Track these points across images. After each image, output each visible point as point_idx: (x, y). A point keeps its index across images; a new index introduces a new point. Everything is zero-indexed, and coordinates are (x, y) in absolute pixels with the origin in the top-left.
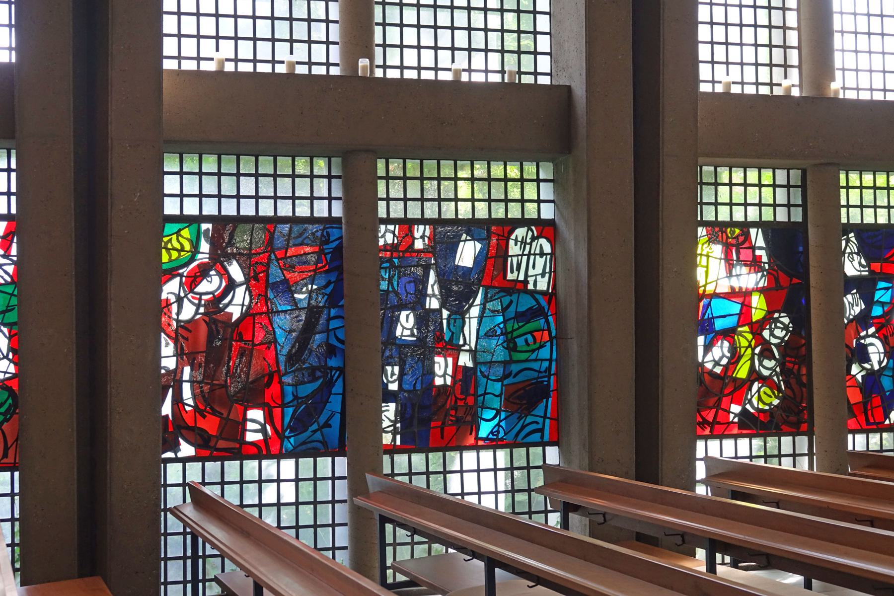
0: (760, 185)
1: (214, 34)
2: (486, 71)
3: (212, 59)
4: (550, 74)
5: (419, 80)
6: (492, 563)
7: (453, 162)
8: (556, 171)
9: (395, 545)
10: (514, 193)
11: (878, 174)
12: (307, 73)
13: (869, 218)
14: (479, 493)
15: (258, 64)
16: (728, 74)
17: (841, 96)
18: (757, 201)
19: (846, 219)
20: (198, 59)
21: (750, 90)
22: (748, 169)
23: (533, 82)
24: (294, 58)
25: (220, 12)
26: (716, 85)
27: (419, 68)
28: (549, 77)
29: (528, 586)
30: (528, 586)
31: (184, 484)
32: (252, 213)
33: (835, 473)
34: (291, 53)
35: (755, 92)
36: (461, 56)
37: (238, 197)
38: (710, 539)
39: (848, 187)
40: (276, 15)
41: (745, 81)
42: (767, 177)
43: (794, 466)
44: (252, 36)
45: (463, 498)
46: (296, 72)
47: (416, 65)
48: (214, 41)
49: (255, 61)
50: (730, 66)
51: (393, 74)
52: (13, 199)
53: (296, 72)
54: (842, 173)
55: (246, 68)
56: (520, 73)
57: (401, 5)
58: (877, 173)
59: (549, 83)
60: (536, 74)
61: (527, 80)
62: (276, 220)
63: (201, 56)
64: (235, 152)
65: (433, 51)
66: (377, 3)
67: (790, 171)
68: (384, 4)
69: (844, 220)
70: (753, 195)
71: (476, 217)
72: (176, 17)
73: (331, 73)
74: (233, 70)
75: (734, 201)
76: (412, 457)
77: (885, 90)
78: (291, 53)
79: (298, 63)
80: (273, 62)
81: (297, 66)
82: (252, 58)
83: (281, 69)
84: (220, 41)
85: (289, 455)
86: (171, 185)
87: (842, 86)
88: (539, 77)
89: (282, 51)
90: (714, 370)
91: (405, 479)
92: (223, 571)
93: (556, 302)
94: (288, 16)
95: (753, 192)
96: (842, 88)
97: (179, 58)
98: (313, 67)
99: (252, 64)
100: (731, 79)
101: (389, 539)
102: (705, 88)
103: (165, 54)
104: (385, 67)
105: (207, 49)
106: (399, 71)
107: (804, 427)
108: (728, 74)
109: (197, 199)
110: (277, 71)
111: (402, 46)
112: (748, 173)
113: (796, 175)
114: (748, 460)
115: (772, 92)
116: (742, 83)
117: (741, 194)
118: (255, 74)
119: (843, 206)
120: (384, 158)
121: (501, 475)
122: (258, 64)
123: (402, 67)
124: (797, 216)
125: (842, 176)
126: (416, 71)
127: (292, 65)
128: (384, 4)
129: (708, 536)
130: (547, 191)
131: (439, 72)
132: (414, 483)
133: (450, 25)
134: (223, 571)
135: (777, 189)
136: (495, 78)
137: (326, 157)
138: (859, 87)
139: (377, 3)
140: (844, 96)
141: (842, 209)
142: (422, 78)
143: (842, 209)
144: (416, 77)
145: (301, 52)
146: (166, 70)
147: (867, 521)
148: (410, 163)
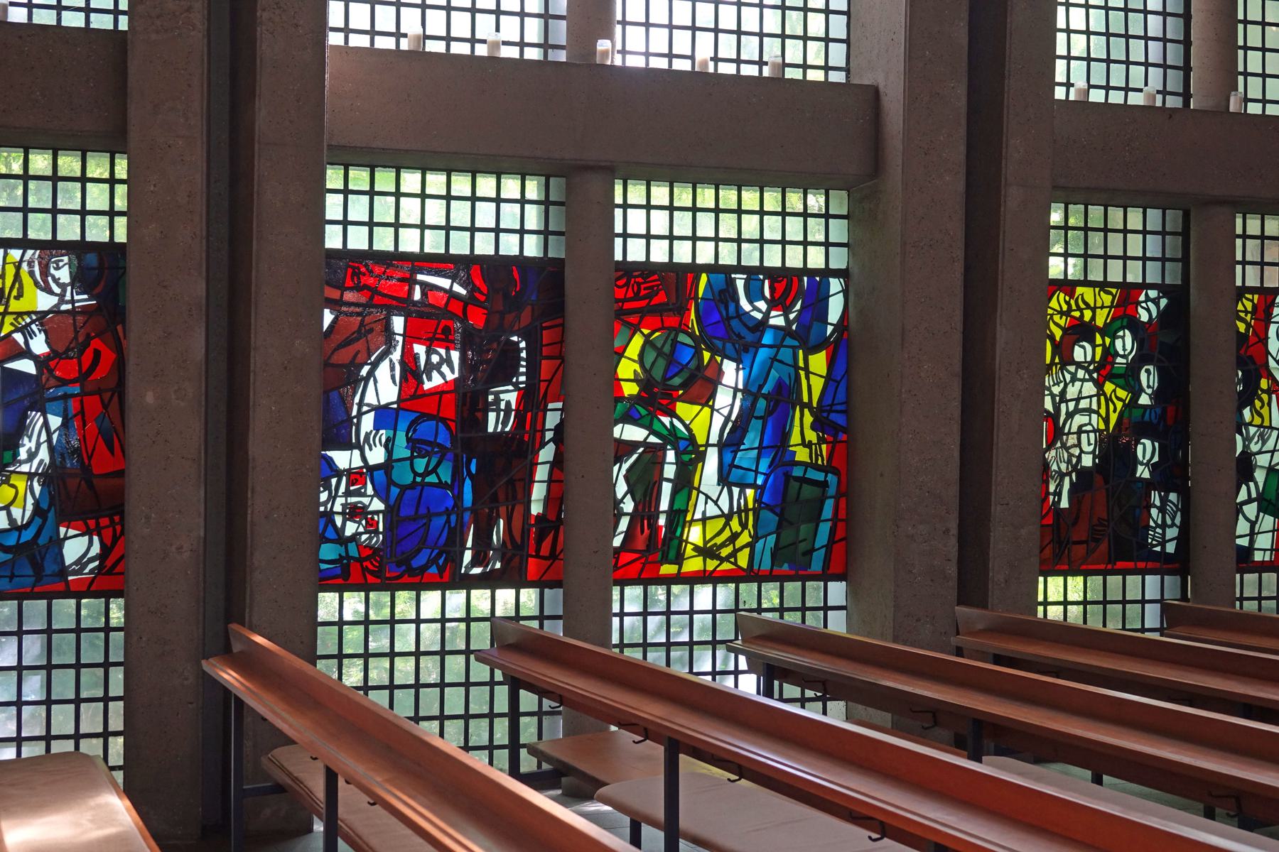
1: (667, 22)
2: (647, 54)
5: (1125, 106)
6: (675, 746)
7: (1102, 208)
13: (484, 246)
15: (742, 66)
17: (711, 70)
19: (116, 224)
21: (816, 76)
24: (504, 36)
28: (844, 74)
32: (415, 248)
33: (868, 637)
34: (498, 30)
36: (705, 40)
39: (1245, 236)
42: (816, 201)
43: (1105, 625)
45: (622, 651)
47: (469, 36)
54: (619, 184)
56: (716, 59)
57: (1087, 6)
58: (89, 154)
61: (436, 47)
64: (1103, 203)
65: (712, 35)
66: (1061, 4)
67: (1167, 211)
68: (1068, 5)
73: (526, 56)
75: (1129, 254)
77: (1264, 101)
78: (498, 30)
79: (505, 43)
80: (473, 41)
81: (11, 9)
83: (481, 50)
84: (628, 27)
86: (333, 209)
87: (713, 56)
88: (453, 44)
91: (535, 624)
93: (847, 389)
95: (773, 224)
96: (712, 59)
98: (377, 38)
99: (734, 65)
106: (734, 65)
107: (484, 564)
109: (493, 235)
110: (1267, 113)
112: (653, 189)
113: (1174, 217)
114: (777, 615)
115: (647, 63)
120: (393, 167)
123: (373, 33)
124: (557, 250)
125: (1239, 221)
126: (517, 49)
127: (495, 46)
128: (1068, 5)
130: (839, 231)
131: (628, 57)
137: (542, 175)
139: (1061, 4)
140: (612, 61)
141: (616, 239)
143: (616, 239)
145: (705, 43)
147: (927, 712)
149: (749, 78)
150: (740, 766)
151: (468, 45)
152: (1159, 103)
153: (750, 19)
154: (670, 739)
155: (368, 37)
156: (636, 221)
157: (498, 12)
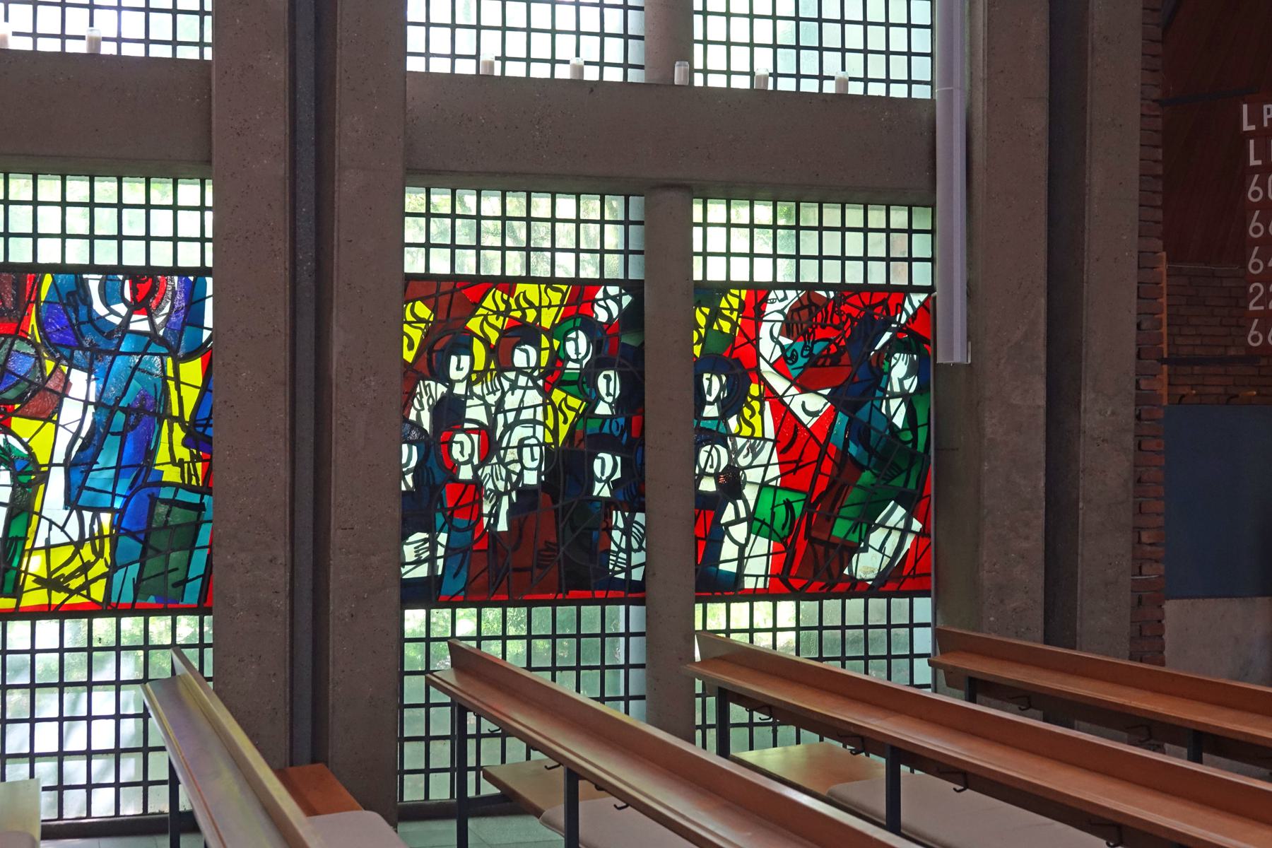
0: (865, 230)
3: (82, 38)
4: (931, 83)
6: (899, 754)
8: (648, 208)
9: (479, 736)
10: (899, 248)
11: (183, 183)
12: (794, 89)
14: (554, 669)
15: (152, 46)
16: (6, 19)
17: (497, 72)
18: (422, 240)
20: (63, 37)
22: (891, 207)
23: (794, 89)
25: (846, 18)
26: (825, 82)
27: (798, 76)
29: (615, 806)
30: (615, 806)
31: (173, 645)
35: (59, 50)
37: (148, 238)
38: (1195, 731)
40: (869, 19)
41: (709, 67)
44: (862, 47)
46: (585, 79)
47: (725, 68)
48: (862, 55)
49: (174, 43)
50: (709, 46)
51: (717, 81)
52: (209, 246)
53: (850, 92)
55: (877, 90)
59: (748, 86)
60: (798, 76)
61: (787, 85)
62: (36, 269)
63: (606, 60)
64: (525, 188)
69: (698, 276)
70: (854, 244)
71: (870, 282)
72: (771, 21)
74: (596, 78)
76: (66, 624)
81: (851, 83)
82: (906, 78)
85: (188, 611)
86: (413, 231)
89: (832, 62)
90: (177, 498)
92: (503, 761)
94: (883, 20)
96: (771, 75)
97: (427, 55)
100: (585, 55)
101: (471, 730)
102: (415, 65)
103: (409, 50)
104: (705, 72)
105: (832, 62)
108: (6, 19)
110: (870, 93)
111: (602, 35)
116: (119, 40)
117: (409, 227)
118: (147, 61)
119: (698, 254)
121: (563, 644)
122: (152, 46)
127: (843, 83)
129: (1194, 727)
132: (483, 649)
133: (905, 22)
134: (503, 761)
135: (914, 236)
136: (742, 83)
138: (123, 36)
142: (151, 55)
144: (724, 85)
146: (411, 72)
148: (783, 207)
149: (786, 94)
150: (965, 774)
151: (30, 40)
152: (497, 72)
153: (565, 18)
154: (893, 748)
155: (142, 46)
156: (717, 239)
157: (174, 12)
